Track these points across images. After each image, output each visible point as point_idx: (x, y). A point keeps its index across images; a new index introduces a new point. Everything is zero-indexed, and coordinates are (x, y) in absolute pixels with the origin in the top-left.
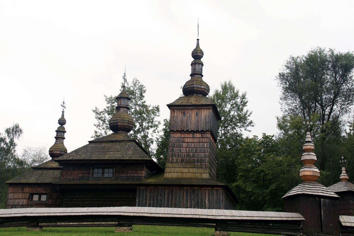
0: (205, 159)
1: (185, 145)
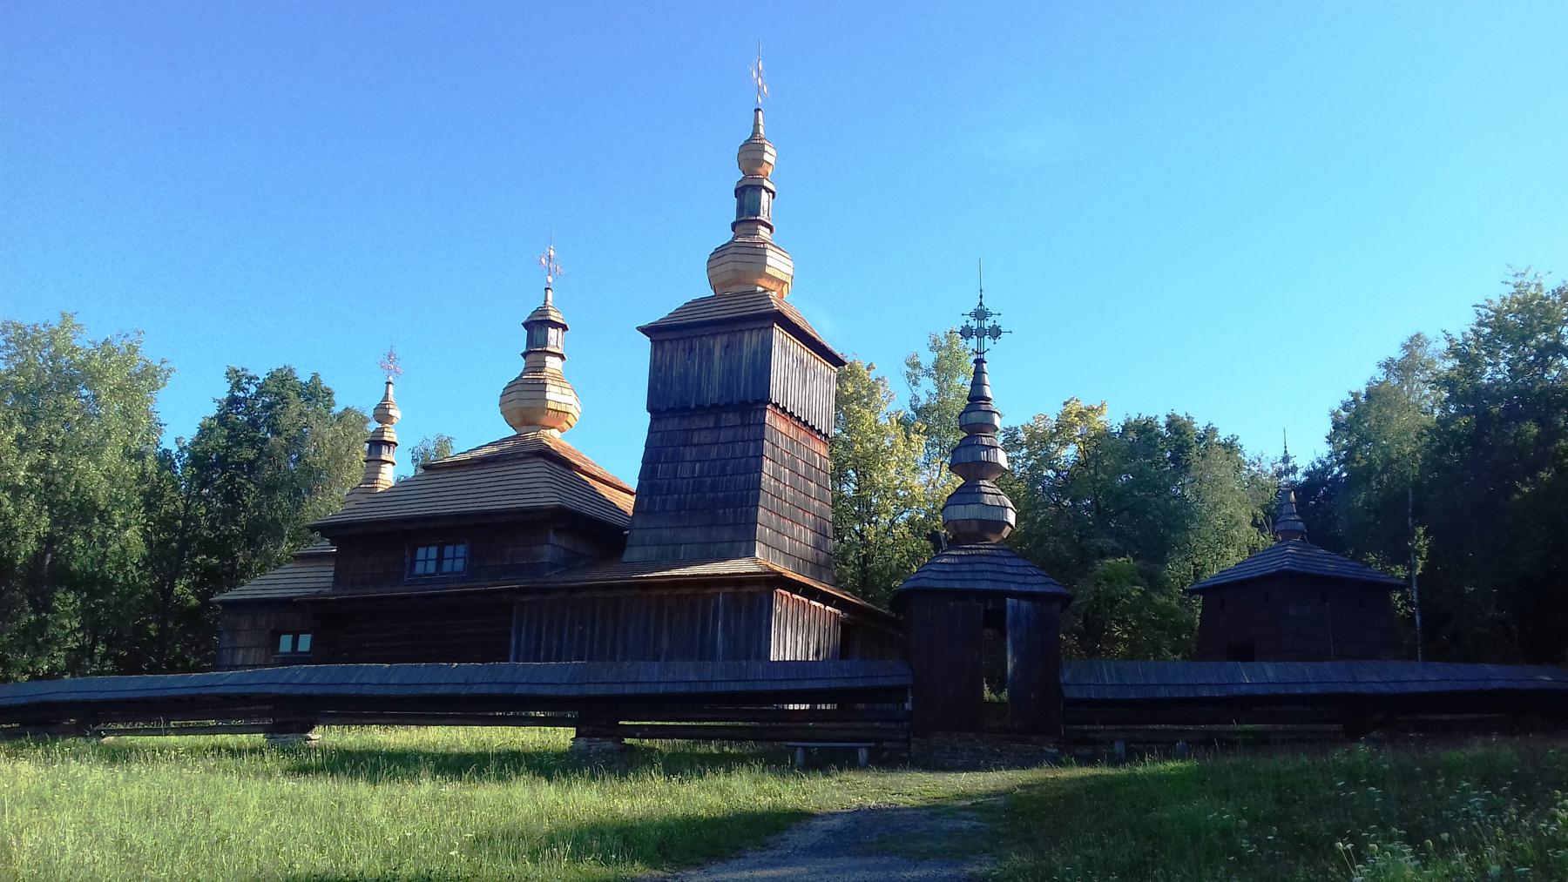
0: (748, 495)
1: (690, 453)
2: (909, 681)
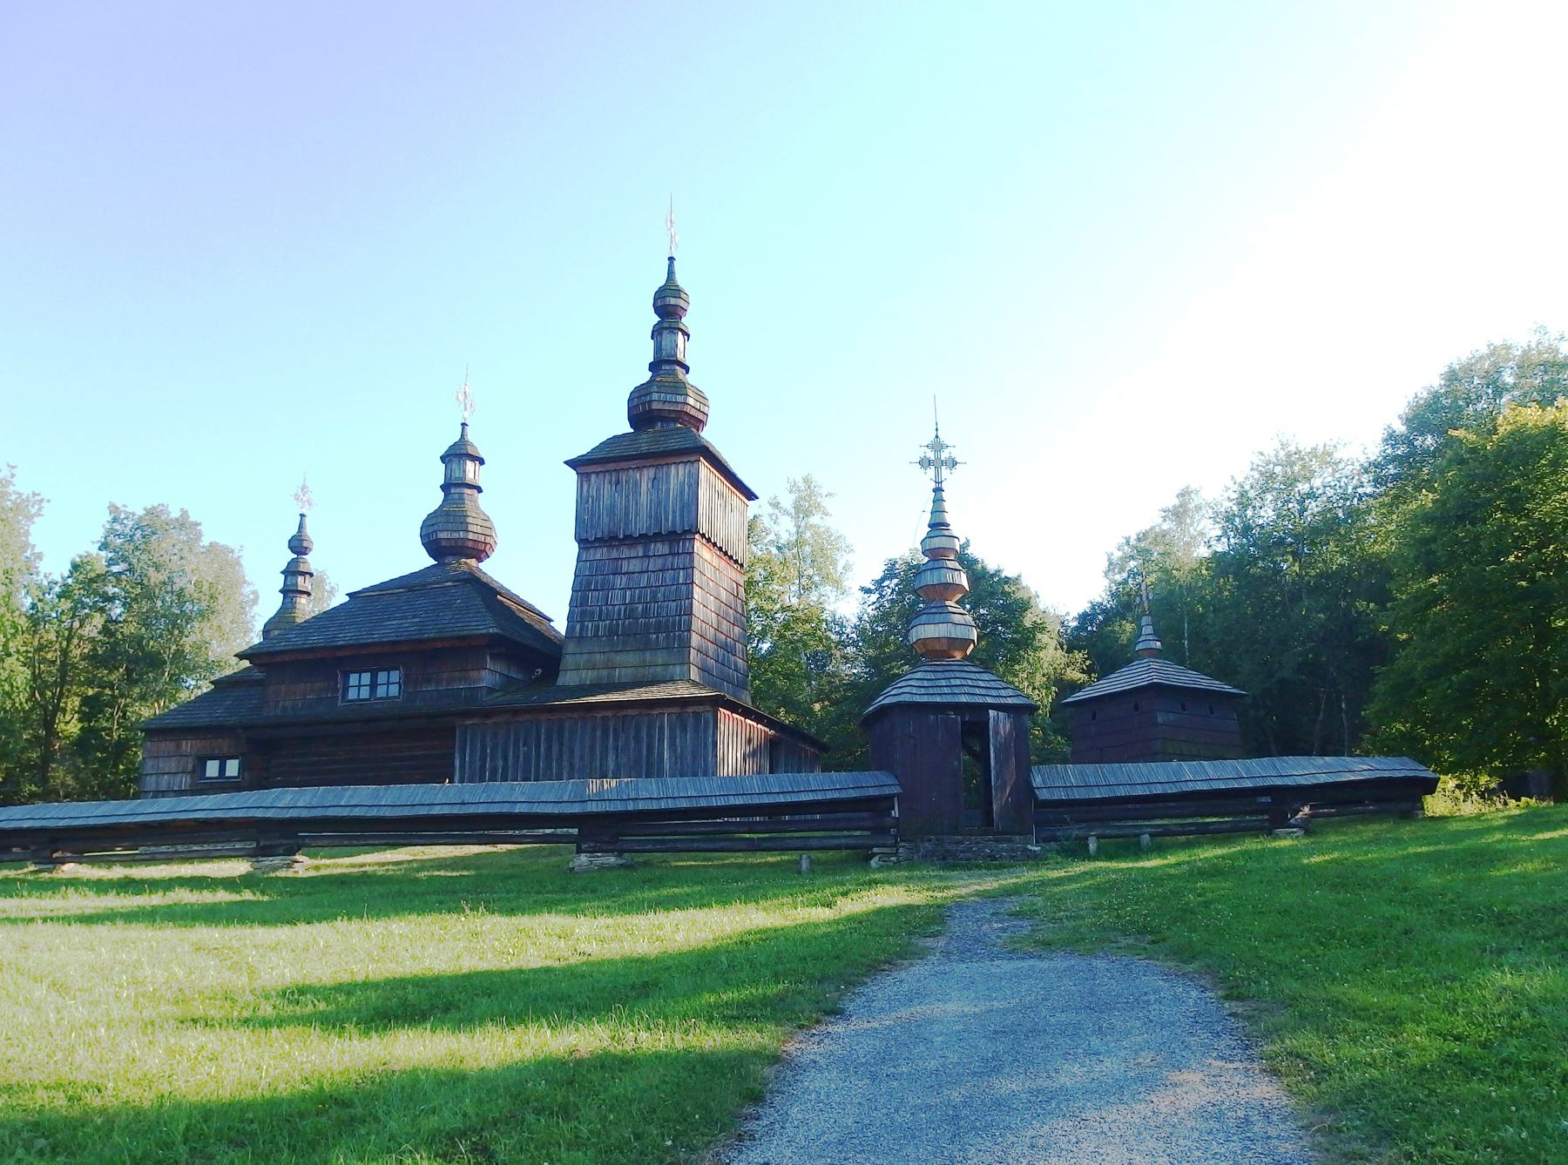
0: (680, 620)
1: (620, 581)
2: (896, 790)
